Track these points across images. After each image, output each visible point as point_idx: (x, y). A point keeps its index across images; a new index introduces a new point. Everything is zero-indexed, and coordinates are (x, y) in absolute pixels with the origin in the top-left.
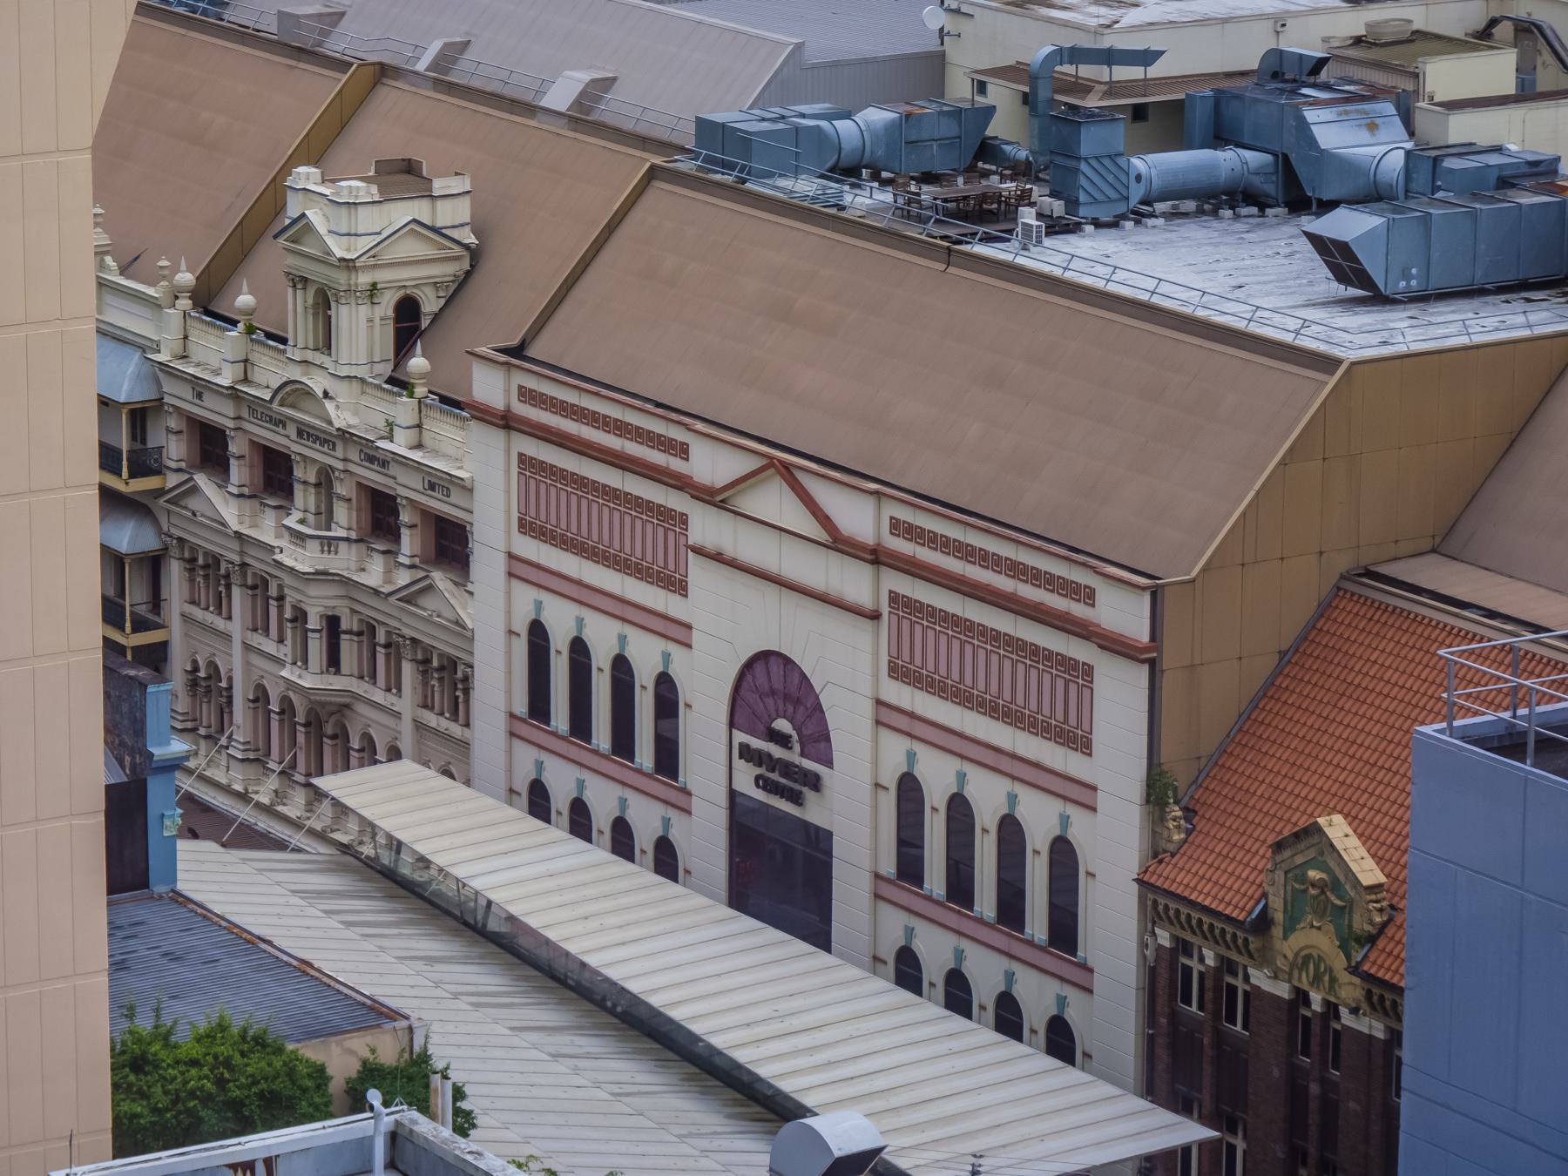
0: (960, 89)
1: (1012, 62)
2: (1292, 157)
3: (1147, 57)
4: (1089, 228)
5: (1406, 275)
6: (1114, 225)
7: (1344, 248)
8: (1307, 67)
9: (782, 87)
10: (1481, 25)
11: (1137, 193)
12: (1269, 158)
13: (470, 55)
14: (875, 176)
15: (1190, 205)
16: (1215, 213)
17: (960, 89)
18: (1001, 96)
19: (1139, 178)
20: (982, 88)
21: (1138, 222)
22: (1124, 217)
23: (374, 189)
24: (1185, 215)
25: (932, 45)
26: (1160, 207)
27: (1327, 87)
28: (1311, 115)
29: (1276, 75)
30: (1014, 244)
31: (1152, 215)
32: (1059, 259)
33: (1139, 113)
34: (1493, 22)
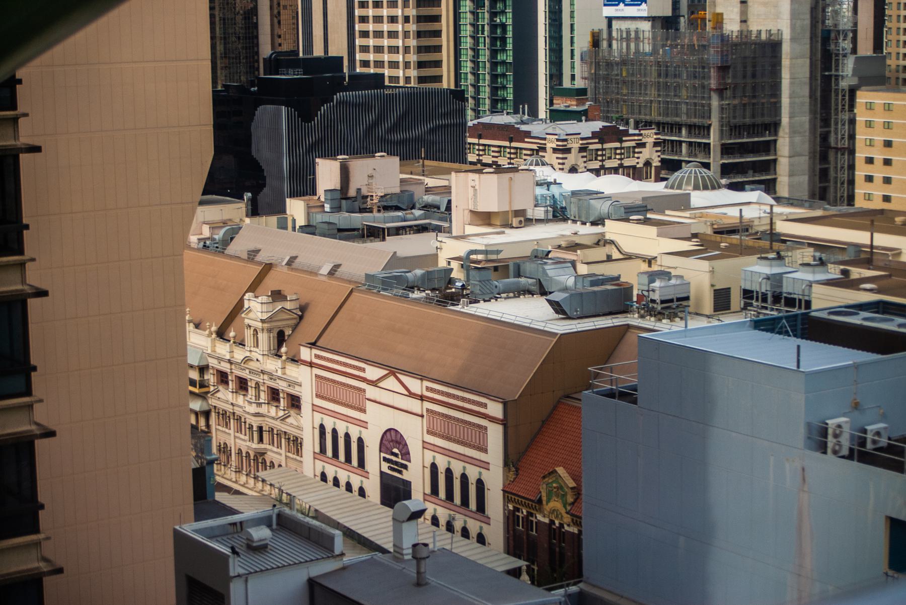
0: (442, 264)
1: (457, 256)
2: (541, 280)
3: (498, 252)
7: (557, 303)
8: (545, 254)
10: (596, 242)
12: (535, 280)
13: (297, 260)
14: (419, 289)
15: (511, 295)
17: (442, 264)
18: (455, 265)
19: (496, 287)
20: (449, 263)
23: (270, 299)
24: (511, 298)
25: (434, 252)
26: (503, 295)
30: (460, 306)
33: (496, 269)
34: (599, 241)
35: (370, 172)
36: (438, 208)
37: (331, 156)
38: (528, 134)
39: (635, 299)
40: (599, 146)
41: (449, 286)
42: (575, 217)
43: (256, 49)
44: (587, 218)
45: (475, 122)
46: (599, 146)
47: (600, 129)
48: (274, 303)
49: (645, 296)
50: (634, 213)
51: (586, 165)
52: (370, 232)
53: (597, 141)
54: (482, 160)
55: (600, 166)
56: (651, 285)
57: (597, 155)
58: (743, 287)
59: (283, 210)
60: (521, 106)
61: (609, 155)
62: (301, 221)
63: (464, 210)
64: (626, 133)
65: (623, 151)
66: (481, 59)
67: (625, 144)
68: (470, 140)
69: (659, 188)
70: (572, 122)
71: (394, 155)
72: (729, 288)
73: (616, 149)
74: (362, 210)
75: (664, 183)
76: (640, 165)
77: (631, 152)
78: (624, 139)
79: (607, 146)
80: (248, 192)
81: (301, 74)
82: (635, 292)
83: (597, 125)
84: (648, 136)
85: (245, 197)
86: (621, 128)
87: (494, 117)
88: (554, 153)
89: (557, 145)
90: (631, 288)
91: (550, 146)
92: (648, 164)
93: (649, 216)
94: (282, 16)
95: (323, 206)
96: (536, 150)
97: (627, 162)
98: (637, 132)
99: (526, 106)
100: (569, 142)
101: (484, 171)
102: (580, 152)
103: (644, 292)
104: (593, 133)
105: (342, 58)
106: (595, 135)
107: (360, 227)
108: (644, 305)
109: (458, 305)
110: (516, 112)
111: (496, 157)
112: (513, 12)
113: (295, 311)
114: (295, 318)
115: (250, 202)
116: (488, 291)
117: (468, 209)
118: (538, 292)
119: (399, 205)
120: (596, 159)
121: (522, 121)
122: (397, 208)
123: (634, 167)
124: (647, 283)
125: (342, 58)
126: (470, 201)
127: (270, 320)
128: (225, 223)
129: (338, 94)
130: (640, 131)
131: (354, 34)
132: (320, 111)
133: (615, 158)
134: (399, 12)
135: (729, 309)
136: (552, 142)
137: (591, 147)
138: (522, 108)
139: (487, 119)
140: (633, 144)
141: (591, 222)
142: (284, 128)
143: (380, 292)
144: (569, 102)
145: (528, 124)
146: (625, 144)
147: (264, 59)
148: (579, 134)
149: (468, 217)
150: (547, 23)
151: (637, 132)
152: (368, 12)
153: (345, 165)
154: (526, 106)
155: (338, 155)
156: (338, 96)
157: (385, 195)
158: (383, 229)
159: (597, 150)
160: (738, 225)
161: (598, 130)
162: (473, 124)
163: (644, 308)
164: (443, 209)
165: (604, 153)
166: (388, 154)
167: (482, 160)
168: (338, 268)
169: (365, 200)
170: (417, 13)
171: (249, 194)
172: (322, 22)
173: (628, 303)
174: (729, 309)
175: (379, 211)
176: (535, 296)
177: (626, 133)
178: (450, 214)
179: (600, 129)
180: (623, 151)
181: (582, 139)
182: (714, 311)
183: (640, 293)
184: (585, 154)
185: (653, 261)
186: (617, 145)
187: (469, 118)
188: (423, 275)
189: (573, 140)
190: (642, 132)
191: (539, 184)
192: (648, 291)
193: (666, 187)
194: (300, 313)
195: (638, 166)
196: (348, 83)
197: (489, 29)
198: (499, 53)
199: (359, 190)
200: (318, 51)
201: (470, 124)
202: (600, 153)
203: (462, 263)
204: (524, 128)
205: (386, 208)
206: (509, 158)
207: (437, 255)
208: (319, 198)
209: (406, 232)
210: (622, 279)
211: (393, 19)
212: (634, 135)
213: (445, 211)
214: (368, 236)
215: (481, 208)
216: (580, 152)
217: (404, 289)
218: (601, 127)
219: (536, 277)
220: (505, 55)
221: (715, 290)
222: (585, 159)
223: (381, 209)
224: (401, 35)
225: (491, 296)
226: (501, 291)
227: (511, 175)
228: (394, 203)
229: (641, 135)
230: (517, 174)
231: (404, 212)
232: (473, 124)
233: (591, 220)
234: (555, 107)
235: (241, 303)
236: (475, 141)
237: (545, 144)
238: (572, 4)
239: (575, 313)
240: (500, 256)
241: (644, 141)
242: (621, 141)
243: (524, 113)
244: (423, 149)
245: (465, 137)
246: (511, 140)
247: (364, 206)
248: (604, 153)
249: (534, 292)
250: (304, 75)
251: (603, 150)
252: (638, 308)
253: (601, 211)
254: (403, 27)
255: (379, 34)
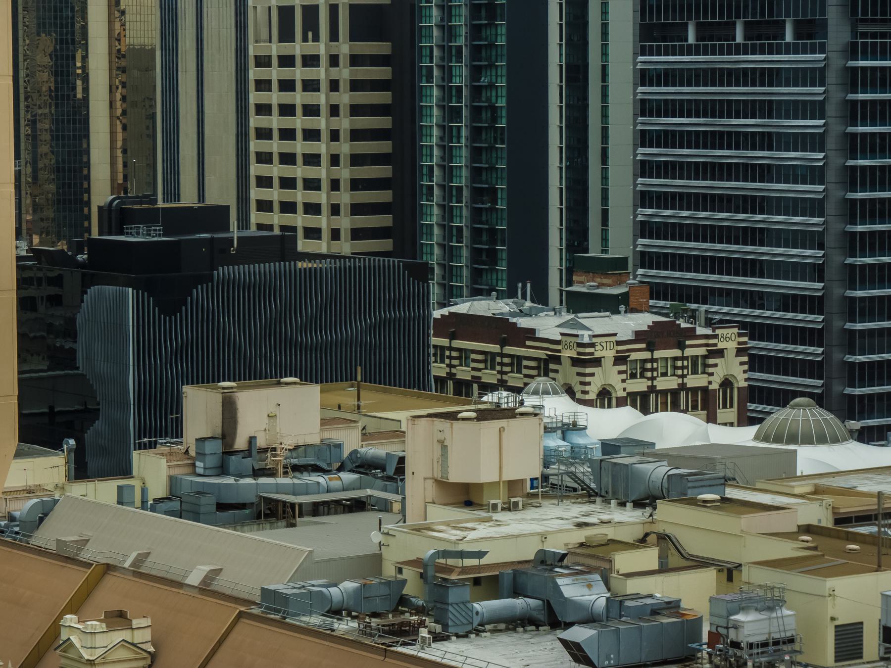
0: (389, 571)
1: (414, 558)
2: (552, 602)
3: (480, 555)
4: (454, 638)
5: (609, 659)
6: (466, 636)
7: (577, 646)
8: (558, 558)
9: (303, 572)
10: (641, 536)
11: (476, 621)
12: (539, 602)
13: (150, 559)
14: (349, 615)
15: (502, 626)
16: (514, 630)
17: (389, 571)
18: (409, 574)
19: (477, 613)
20: (400, 571)
21: (477, 635)
22: (470, 632)
23: (104, 625)
24: (500, 631)
25: (376, 550)
26: (488, 627)
27: (567, 567)
28: (560, 581)
29: (543, 562)
30: (417, 647)
31: (484, 631)
32: (439, 653)
33: (477, 581)
34: (647, 535)
35: (273, 410)
36: (383, 469)
37: (208, 382)
38: (530, 333)
39: (705, 638)
40: (647, 355)
41: (400, 608)
42: (607, 492)
43: (85, 172)
44: (626, 495)
45: (445, 311)
46: (647, 355)
47: (649, 326)
48: (110, 634)
49: (721, 635)
50: (704, 489)
51: (624, 385)
52: (269, 509)
53: (643, 346)
54: (455, 374)
55: (648, 387)
56: (732, 618)
57: (644, 370)
58: (883, 623)
59: (125, 471)
60: (520, 285)
61: (664, 371)
62: (158, 489)
63: (425, 479)
64: (691, 334)
65: (685, 363)
66: (456, 82)
67: (689, 352)
68: (435, 341)
69: (745, 436)
70: (602, 314)
71: (311, 382)
72: (861, 623)
73: (675, 359)
74: (257, 473)
75: (753, 430)
76: (715, 386)
77: (698, 365)
78: (688, 343)
79: (658, 354)
80: (70, 437)
81: (160, 235)
82: (706, 629)
83: (643, 321)
84: (727, 339)
85: (65, 447)
86: (684, 325)
87: (475, 303)
88: (573, 365)
89: (579, 353)
90: (699, 621)
91: (567, 353)
92: (727, 384)
93: (731, 493)
94: (127, 16)
95: (194, 465)
96: (545, 360)
97: (695, 381)
98: (709, 331)
99: (529, 285)
100: (597, 348)
101: (460, 415)
102: (615, 364)
103: (719, 629)
104: (637, 333)
105: (228, 207)
106: (639, 336)
107: (254, 500)
108: (720, 650)
109: (415, 645)
110: (511, 293)
111: (479, 370)
112: (509, 67)
113: (143, 646)
114: (144, 658)
115: (73, 455)
116: (465, 621)
117: (432, 478)
118: (546, 623)
119: (318, 463)
120: (642, 376)
121: (521, 311)
122: (316, 469)
123: (705, 390)
124: (724, 614)
125: (228, 207)
126: (435, 463)
127: (103, 661)
128: (30, 491)
129: (220, 269)
130: (714, 331)
131: (247, 135)
132: (191, 295)
133: (674, 375)
134: (321, 48)
135: (861, 657)
136: (570, 347)
137: (634, 356)
138: (522, 289)
139: (463, 307)
140: (702, 351)
141: (633, 501)
142: (131, 324)
143: (285, 618)
144: (599, 280)
145: (531, 316)
146: (689, 352)
147: (100, 208)
148: (615, 335)
149: (431, 490)
150: (564, 166)
151: (709, 331)
152: (271, 121)
153: (230, 397)
154: (529, 285)
155: (219, 382)
156: (223, 272)
157: (296, 448)
158: (293, 505)
159: (645, 361)
160: (876, 507)
161: (646, 328)
162: (442, 315)
163: (720, 655)
164: (391, 471)
165: (655, 365)
166: (301, 380)
167: (455, 374)
168: (218, 575)
169: (263, 456)
170: (351, 149)
171: (72, 442)
172: (195, 136)
173: (694, 646)
174: (861, 657)
175: (286, 473)
176: (541, 628)
177: (691, 334)
178: (403, 480)
179: (649, 326)
180: (685, 363)
181: (619, 343)
182: (836, 661)
183: (714, 630)
184: (623, 368)
185: (735, 573)
186: (677, 353)
187: (434, 298)
188: (357, 591)
189: (604, 345)
190: (718, 332)
191: (548, 430)
192: (727, 628)
193: (757, 438)
194: (152, 649)
195: (711, 387)
196: (237, 250)
197: (468, 255)
198: (483, 73)
199: (252, 440)
200: (188, 198)
201: (437, 314)
202: (649, 366)
203: (422, 571)
204: (523, 322)
205: (297, 469)
206: (499, 372)
207: (381, 555)
208: (187, 451)
209: (329, 509)
210: (683, 605)
211: (311, 61)
212: (707, 337)
213: (395, 474)
214: (267, 516)
215: (455, 477)
216: (615, 364)
217: (323, 615)
218: (651, 324)
219: (544, 598)
220: (494, 73)
221: (836, 627)
222: (624, 376)
223: (289, 470)
224: (325, 210)
225: (469, 628)
226: (485, 620)
227: (503, 423)
228: (311, 460)
229: (716, 337)
230: (513, 422)
231: (326, 477)
232: (442, 315)
233: (634, 498)
234: (575, 288)
235: (55, 629)
236: (444, 342)
237: (559, 351)
238: (605, 6)
239: (607, 662)
240: (485, 561)
241: (720, 346)
242: (682, 346)
243: (524, 297)
244: (359, 368)
245: (429, 335)
246: (503, 343)
247: (261, 465)
248: (655, 365)
249: (540, 621)
250: (164, 236)
251: (653, 360)
252: (710, 655)
253: (651, 486)
254: (328, 198)
255: (288, 159)
